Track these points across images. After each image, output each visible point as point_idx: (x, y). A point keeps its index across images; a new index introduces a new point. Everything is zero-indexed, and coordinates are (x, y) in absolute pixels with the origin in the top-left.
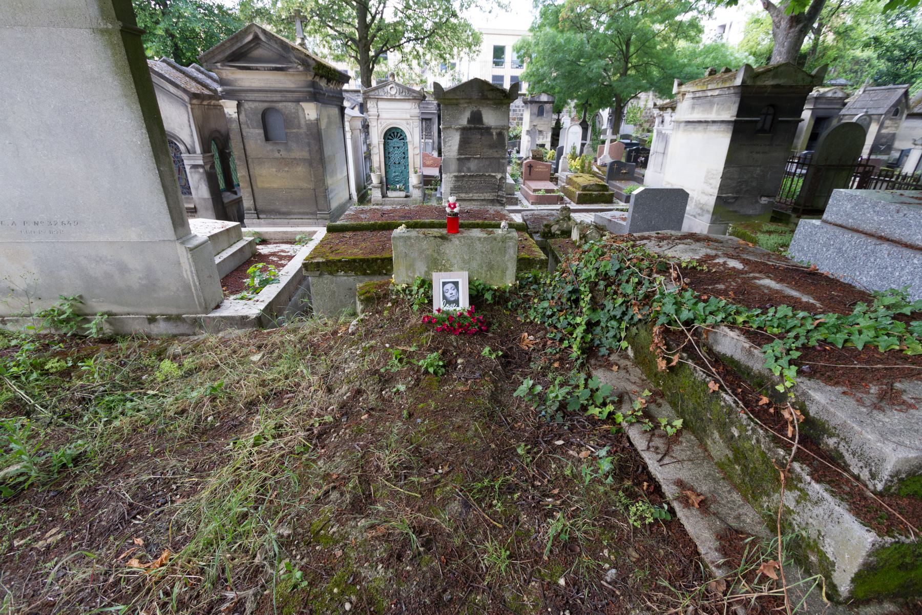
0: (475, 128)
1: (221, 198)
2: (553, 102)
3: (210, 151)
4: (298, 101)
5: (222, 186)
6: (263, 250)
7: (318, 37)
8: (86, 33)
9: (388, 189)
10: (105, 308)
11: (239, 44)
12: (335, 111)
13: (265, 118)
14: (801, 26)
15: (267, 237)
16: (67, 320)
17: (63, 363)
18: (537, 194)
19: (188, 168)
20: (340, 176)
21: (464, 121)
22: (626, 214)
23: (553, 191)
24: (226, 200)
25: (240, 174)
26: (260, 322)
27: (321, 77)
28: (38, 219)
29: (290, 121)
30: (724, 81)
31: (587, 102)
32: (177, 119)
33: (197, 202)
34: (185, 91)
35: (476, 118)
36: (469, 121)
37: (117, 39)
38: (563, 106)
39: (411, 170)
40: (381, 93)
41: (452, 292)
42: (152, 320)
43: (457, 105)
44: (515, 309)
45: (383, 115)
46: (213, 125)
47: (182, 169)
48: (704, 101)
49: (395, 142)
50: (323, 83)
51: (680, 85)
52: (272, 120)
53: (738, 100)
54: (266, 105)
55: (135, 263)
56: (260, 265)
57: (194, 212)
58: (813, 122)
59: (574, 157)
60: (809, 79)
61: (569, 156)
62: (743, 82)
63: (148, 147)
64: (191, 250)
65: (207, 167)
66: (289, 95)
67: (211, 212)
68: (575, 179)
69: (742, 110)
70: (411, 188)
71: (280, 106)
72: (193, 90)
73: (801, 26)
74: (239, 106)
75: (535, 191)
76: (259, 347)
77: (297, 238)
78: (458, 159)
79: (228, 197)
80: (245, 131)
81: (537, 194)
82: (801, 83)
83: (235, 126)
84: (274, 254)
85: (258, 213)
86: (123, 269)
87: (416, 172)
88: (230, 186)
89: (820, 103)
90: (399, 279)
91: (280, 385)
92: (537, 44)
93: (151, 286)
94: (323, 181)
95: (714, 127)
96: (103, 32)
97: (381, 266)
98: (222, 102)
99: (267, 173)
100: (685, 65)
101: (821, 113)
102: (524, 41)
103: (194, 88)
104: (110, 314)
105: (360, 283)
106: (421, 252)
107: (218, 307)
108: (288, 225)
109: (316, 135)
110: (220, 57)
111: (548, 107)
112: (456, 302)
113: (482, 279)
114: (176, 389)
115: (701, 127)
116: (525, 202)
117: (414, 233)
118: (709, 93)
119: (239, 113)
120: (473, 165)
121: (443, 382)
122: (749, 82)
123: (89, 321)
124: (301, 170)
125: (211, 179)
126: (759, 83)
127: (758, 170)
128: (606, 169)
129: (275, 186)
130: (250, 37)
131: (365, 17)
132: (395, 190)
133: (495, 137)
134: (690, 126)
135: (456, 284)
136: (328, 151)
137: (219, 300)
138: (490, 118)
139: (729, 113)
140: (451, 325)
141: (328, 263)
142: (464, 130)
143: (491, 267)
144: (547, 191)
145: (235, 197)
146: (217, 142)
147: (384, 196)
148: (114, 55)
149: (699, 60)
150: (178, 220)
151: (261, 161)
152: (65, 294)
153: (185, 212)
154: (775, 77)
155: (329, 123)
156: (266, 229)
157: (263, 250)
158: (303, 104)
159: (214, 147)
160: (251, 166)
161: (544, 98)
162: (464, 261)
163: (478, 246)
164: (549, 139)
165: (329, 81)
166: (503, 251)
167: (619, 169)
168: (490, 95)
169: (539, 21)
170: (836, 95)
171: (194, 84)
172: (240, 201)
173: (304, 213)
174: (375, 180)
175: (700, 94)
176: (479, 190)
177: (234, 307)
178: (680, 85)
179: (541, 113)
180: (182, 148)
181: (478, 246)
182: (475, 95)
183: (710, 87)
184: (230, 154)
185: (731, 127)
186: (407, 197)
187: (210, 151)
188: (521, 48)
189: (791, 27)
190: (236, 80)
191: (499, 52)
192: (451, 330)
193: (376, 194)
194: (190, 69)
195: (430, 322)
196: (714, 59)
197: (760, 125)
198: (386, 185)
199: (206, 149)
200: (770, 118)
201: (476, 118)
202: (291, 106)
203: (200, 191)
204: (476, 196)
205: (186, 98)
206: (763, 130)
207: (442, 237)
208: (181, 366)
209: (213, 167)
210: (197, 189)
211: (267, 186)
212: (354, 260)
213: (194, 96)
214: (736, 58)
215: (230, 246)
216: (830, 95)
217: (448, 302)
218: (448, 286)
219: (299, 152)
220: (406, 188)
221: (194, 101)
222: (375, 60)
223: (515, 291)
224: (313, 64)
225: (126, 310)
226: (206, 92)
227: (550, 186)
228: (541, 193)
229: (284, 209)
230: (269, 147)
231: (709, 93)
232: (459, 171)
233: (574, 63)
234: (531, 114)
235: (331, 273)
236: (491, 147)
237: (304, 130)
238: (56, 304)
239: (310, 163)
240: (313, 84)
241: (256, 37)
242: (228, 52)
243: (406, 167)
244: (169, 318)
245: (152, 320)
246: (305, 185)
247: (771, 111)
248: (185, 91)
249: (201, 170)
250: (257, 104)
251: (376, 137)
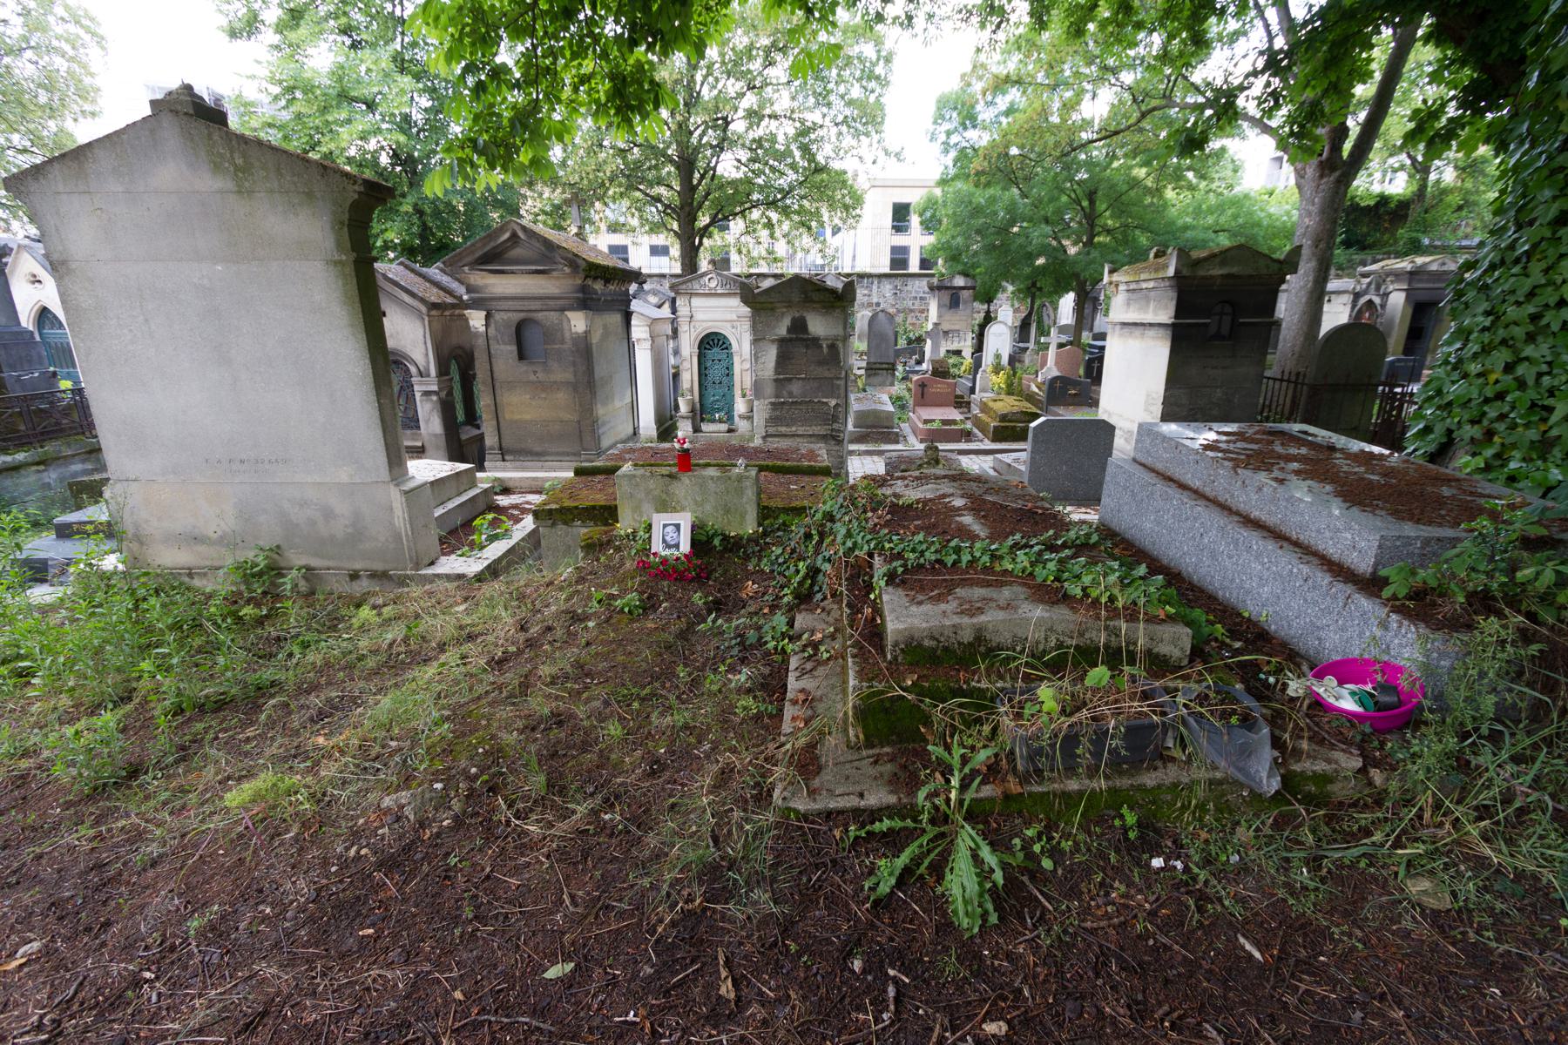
0: (797, 339)
1: (458, 434)
2: (973, 288)
3: (447, 374)
4: (563, 310)
5: (460, 416)
6: (503, 501)
7: (625, 203)
8: (319, 265)
9: (702, 420)
10: (302, 562)
11: (493, 244)
12: (616, 318)
13: (520, 332)
14: (1337, 174)
15: (511, 485)
16: (260, 574)
17: (257, 611)
18: (928, 426)
19: (418, 396)
20: (621, 402)
21: (782, 331)
22: (1023, 456)
23: (954, 422)
24: (464, 437)
25: (483, 402)
26: (479, 578)
27: (595, 278)
28: (244, 457)
29: (552, 335)
30: (1156, 270)
31: (1034, 284)
32: (408, 334)
33: (426, 438)
34: (422, 300)
35: (799, 326)
36: (789, 331)
37: (350, 269)
38: (996, 291)
39: (737, 392)
40: (696, 286)
41: (671, 534)
42: (354, 576)
43: (772, 309)
44: (747, 558)
45: (699, 316)
46: (455, 340)
47: (411, 398)
48: (1139, 295)
49: (715, 353)
50: (598, 286)
51: (1111, 272)
52: (531, 335)
53: (1175, 295)
54: (522, 315)
55: (342, 508)
56: (490, 516)
57: (420, 452)
58: (1410, 311)
59: (997, 369)
60: (1276, 266)
61: (990, 369)
62: (1177, 272)
63: (370, 378)
64: (406, 492)
65: (443, 394)
66: (551, 303)
67: (443, 452)
68: (991, 404)
69: (1179, 313)
70: (736, 418)
71: (540, 316)
72: (433, 299)
73: (1337, 174)
74: (488, 317)
75: (926, 422)
76: (466, 599)
77: (547, 485)
78: (776, 380)
79: (468, 433)
80: (494, 347)
81: (928, 426)
82: (1264, 271)
83: (481, 342)
84: (515, 507)
85: (504, 453)
86: (329, 514)
87: (744, 396)
88: (472, 418)
89: (1420, 281)
90: (624, 526)
91: (477, 630)
92: (945, 204)
93: (357, 535)
94: (591, 411)
95: (1151, 332)
96: (336, 263)
97: (608, 514)
98: (466, 312)
99: (519, 402)
100: (1186, 228)
101: (1423, 297)
102: (929, 200)
103: (434, 296)
104: (309, 569)
105: (582, 531)
106: (648, 492)
107: (432, 563)
108: (542, 469)
109: (584, 350)
110: (469, 259)
111: (965, 294)
112: (677, 546)
113: (715, 522)
114: (372, 627)
115: (1138, 331)
116: (912, 440)
117: (641, 471)
118: (1144, 285)
119: (487, 325)
120: (796, 388)
121: (632, 621)
122: (1185, 272)
123: (283, 576)
124: (562, 396)
125: (447, 409)
126: (1201, 273)
127: (1219, 393)
128: (1045, 388)
129: (528, 417)
130: (507, 235)
131: (691, 177)
132: (713, 421)
133: (825, 350)
134: (1126, 330)
135: (678, 527)
136: (600, 370)
137: (433, 556)
138: (818, 326)
139: (1164, 313)
140: (669, 572)
141: (563, 511)
142: (782, 342)
143: (727, 511)
144: (945, 422)
145: (477, 432)
146: (457, 362)
147: (697, 430)
148: (344, 285)
149: (1210, 220)
150: (396, 459)
151: (511, 385)
152: (261, 543)
153: (403, 450)
154: (1223, 263)
155: (606, 334)
156: (510, 474)
157: (503, 501)
158: (569, 314)
159: (454, 368)
160: (498, 392)
161: (959, 281)
162: (696, 502)
163: (711, 485)
164: (969, 342)
165: (607, 281)
166: (740, 492)
167: (1064, 389)
168: (815, 296)
169: (952, 172)
170: (1445, 268)
171: (435, 290)
172: (481, 438)
173: (563, 454)
174: (684, 408)
175: (1132, 286)
176: (805, 422)
177: (452, 564)
178: (1111, 272)
179: (954, 303)
180: (413, 370)
181: (711, 485)
182: (796, 297)
183: (1143, 277)
184: (474, 376)
185: (1169, 333)
186: (730, 431)
187: (447, 374)
188: (924, 211)
189: (1322, 176)
190: (486, 286)
191: (901, 214)
192: (663, 575)
193: (684, 429)
194: (434, 271)
195: (644, 566)
196: (1235, 217)
197: (1213, 330)
198: (700, 414)
199: (443, 371)
200: (1227, 320)
201: (799, 326)
202: (553, 316)
203: (431, 423)
204: (801, 430)
205: (424, 309)
206: (1218, 336)
207: (671, 476)
208: (379, 615)
209: (450, 393)
210: (427, 421)
211: (517, 417)
212: (594, 507)
213: (434, 306)
214: (1270, 216)
215: (459, 494)
216: (1434, 267)
217: (669, 546)
218: (669, 529)
219: (562, 374)
220: (730, 418)
221: (434, 313)
222: (705, 231)
223: (753, 540)
224: (583, 265)
225: (331, 564)
226: (449, 300)
227: (955, 414)
228: (935, 426)
229: (538, 449)
230: (523, 367)
231: (1144, 285)
232: (777, 396)
233: (1004, 230)
234: (940, 306)
235: (565, 523)
236: (821, 363)
237: (568, 345)
238: (250, 555)
239: (575, 387)
240: (583, 289)
241: (514, 235)
242: (478, 254)
243: (731, 387)
244: (374, 575)
245: (354, 576)
246: (567, 417)
247: (1228, 309)
248: (422, 300)
249: (435, 398)
250: (510, 314)
251: (688, 345)
